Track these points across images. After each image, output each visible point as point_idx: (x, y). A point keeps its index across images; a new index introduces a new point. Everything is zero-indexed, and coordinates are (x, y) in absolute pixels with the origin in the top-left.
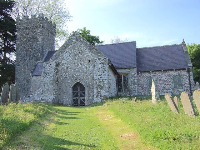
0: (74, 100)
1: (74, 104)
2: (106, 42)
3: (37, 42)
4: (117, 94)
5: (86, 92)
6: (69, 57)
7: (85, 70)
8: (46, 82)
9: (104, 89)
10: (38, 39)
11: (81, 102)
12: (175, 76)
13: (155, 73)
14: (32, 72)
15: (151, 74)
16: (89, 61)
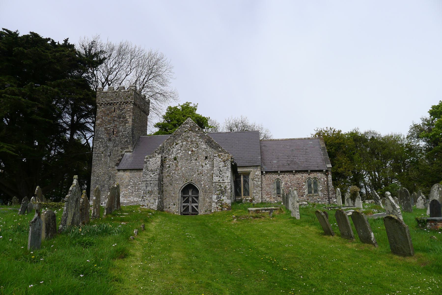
0: (184, 206)
1: (183, 211)
2: (223, 128)
3: (126, 123)
4: (235, 200)
5: (200, 198)
6: (179, 151)
7: (201, 168)
8: (148, 182)
9: (226, 194)
10: (126, 120)
11: (193, 209)
12: (309, 178)
13: (284, 174)
14: (117, 165)
15: (279, 175)
16: (206, 158)
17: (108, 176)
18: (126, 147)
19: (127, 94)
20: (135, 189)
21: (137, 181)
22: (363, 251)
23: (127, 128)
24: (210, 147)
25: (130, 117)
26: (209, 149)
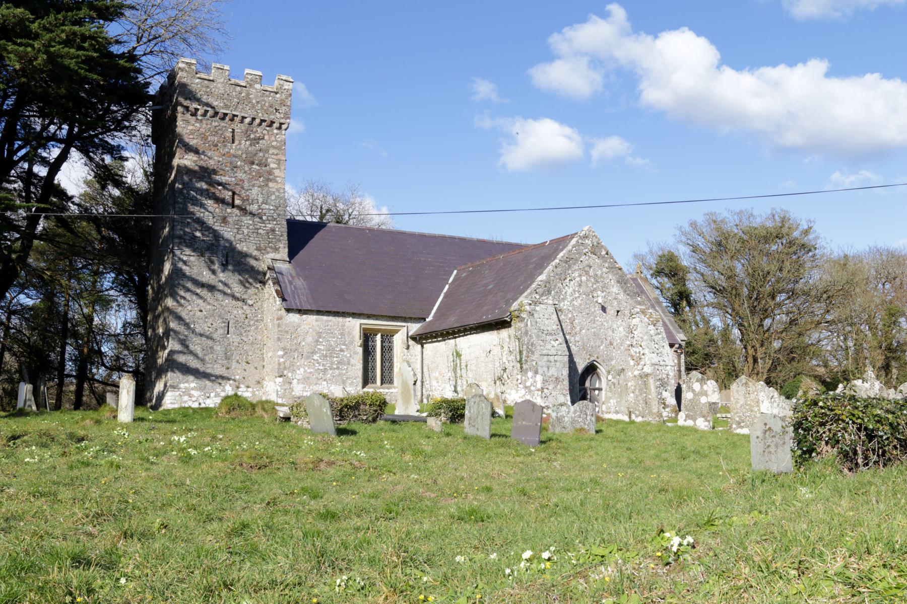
3: (269, 180)
7: (610, 333)
10: (270, 173)
17: (224, 322)
18: (271, 248)
19: (270, 98)
20: (332, 363)
21: (336, 341)
22: (42, 495)
23: (271, 195)
24: (625, 292)
25: (279, 164)
26: (622, 296)
